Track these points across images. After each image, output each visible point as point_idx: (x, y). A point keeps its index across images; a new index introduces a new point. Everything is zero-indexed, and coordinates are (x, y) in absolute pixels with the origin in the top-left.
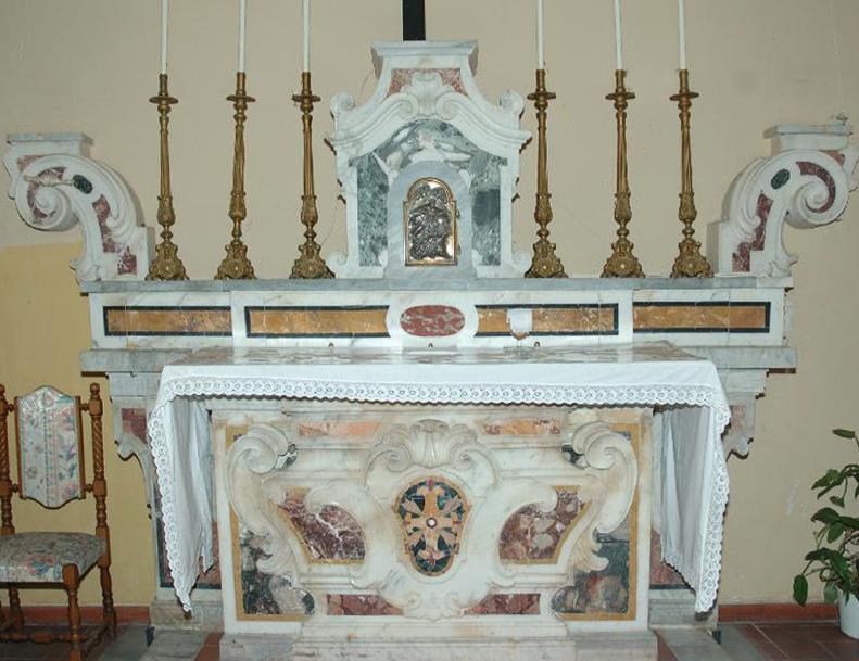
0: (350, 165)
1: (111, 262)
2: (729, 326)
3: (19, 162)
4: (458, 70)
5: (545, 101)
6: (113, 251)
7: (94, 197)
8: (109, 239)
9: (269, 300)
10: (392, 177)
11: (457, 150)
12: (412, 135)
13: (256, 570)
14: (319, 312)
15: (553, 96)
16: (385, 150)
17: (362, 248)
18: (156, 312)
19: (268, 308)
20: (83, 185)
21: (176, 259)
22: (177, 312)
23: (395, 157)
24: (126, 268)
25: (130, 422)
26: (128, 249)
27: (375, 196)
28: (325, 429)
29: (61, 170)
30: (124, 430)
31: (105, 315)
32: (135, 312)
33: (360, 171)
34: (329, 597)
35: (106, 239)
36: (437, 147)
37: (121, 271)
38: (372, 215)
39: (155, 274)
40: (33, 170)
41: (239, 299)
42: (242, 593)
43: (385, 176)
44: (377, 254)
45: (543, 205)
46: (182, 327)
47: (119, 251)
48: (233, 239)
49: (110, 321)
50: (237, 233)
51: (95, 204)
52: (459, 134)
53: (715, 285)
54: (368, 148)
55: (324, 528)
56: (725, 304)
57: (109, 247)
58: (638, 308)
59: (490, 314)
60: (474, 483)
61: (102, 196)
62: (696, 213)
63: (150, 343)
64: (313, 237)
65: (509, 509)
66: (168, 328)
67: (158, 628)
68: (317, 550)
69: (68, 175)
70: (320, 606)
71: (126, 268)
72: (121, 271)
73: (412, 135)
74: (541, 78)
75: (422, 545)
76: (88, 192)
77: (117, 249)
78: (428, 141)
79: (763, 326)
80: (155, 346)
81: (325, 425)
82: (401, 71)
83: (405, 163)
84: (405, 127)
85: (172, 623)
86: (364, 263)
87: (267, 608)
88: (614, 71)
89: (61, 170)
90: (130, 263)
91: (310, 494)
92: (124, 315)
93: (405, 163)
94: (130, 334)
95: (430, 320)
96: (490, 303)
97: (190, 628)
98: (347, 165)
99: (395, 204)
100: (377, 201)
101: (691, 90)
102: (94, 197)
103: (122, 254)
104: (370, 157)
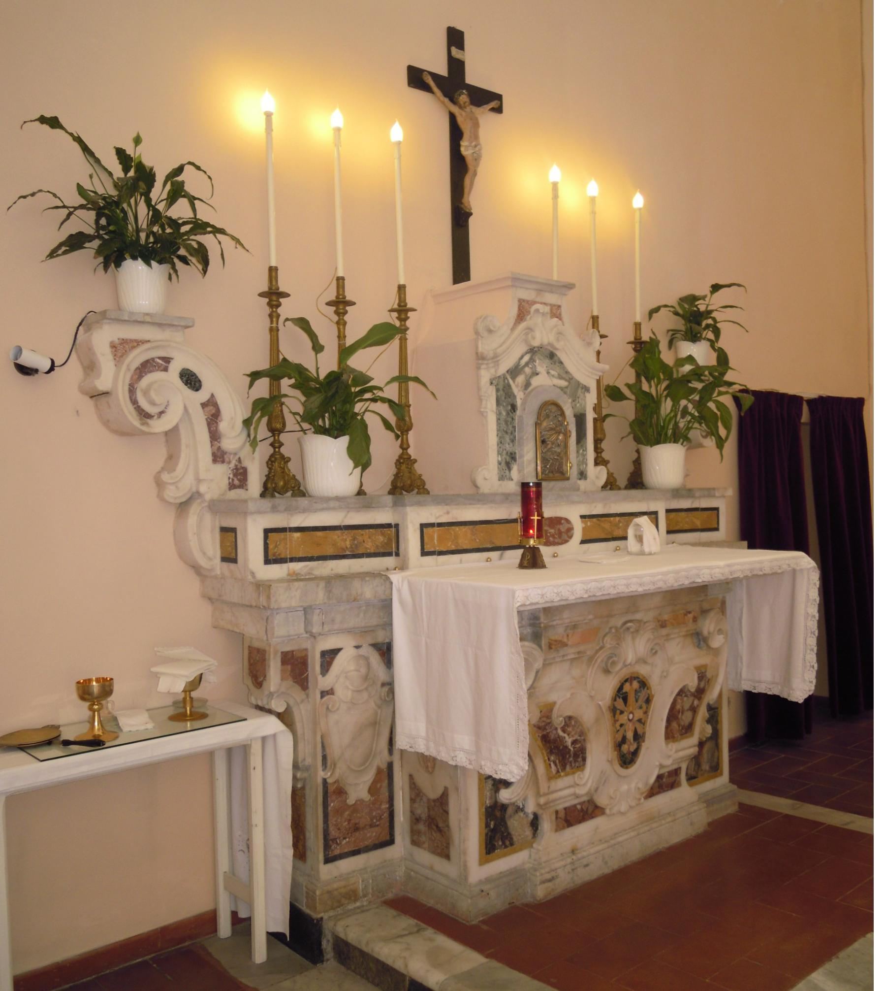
0: (491, 383)
1: (222, 473)
2: (700, 527)
3: (113, 346)
4: (559, 306)
5: (344, 308)
6: (223, 462)
7: (203, 395)
8: (219, 448)
9: (439, 517)
10: (519, 395)
11: (560, 377)
12: (532, 360)
13: (496, 802)
14: (478, 527)
15: (287, 295)
16: (515, 371)
17: (500, 464)
18: (319, 534)
19: (440, 525)
20: (191, 380)
21: (270, 469)
22: (338, 532)
23: (521, 379)
24: (236, 482)
25: (289, 667)
26: (239, 460)
27: (508, 414)
28: (565, 640)
29: (167, 360)
30: (282, 679)
31: (266, 538)
32: (297, 535)
33: (497, 390)
34: (557, 812)
35: (215, 448)
36: (548, 373)
37: (232, 487)
38: (507, 433)
39: (268, 490)
40: (136, 358)
41: (414, 517)
42: (484, 831)
43: (515, 397)
44: (510, 469)
45: (598, 428)
46: (344, 550)
47: (229, 462)
48: (401, 451)
49: (271, 547)
50: (404, 447)
51: (204, 405)
52: (561, 363)
53: (717, 494)
54: (503, 369)
55: (562, 739)
56: (696, 509)
57: (219, 457)
58: (673, 515)
59: (589, 524)
60: (652, 672)
61: (212, 395)
62: (605, 435)
63: (312, 569)
64: (279, 447)
65: (672, 693)
66: (330, 551)
67: (325, 916)
68: (556, 765)
69: (175, 368)
70: (546, 825)
71: (236, 482)
72: (232, 487)
73: (532, 360)
74: (274, 274)
75: (624, 740)
76: (197, 390)
77: (227, 460)
78: (541, 366)
79: (393, 530)
80: (317, 573)
81: (565, 637)
82: (524, 301)
83: (527, 385)
84: (526, 353)
85: (341, 905)
86: (501, 478)
87: (504, 843)
88: (590, 315)
89: (167, 360)
90: (240, 477)
91: (557, 706)
92: (285, 539)
93: (527, 385)
94: (292, 560)
95: (552, 531)
96: (588, 514)
97: (358, 904)
98: (489, 384)
99: (526, 418)
100: (510, 419)
101: (282, 289)
102: (203, 395)
103: (232, 465)
104: (504, 375)
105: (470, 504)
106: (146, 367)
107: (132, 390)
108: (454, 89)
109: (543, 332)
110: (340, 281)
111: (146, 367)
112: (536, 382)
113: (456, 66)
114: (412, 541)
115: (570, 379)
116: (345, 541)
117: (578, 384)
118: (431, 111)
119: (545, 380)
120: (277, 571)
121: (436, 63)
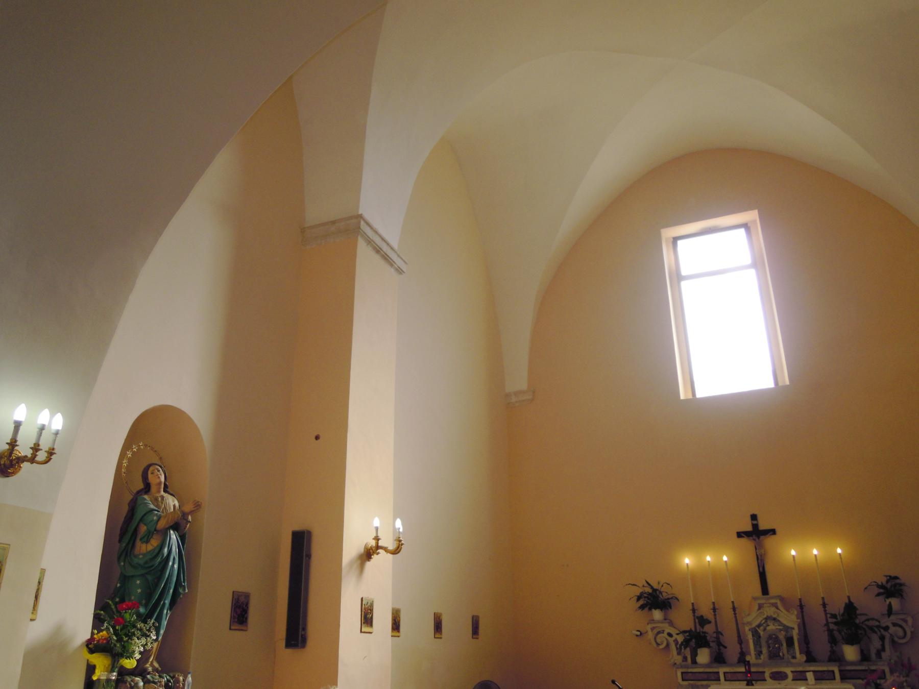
10: (762, 633)
16: (759, 626)
23: (762, 628)
40: (655, 631)
41: (722, 670)
54: (754, 625)
78: (770, 623)
83: (765, 629)
90: (685, 659)
93: (765, 629)
105: (304, 629)
106: (659, 633)
107: (655, 639)
108: (756, 533)
109: (770, 611)
110: (714, 603)
111: (659, 633)
112: (768, 628)
113: (755, 526)
114: (722, 677)
115: (784, 626)
116: (705, 676)
117: (788, 627)
118: (747, 544)
119: (772, 627)
120: (685, 683)
121: (749, 528)
